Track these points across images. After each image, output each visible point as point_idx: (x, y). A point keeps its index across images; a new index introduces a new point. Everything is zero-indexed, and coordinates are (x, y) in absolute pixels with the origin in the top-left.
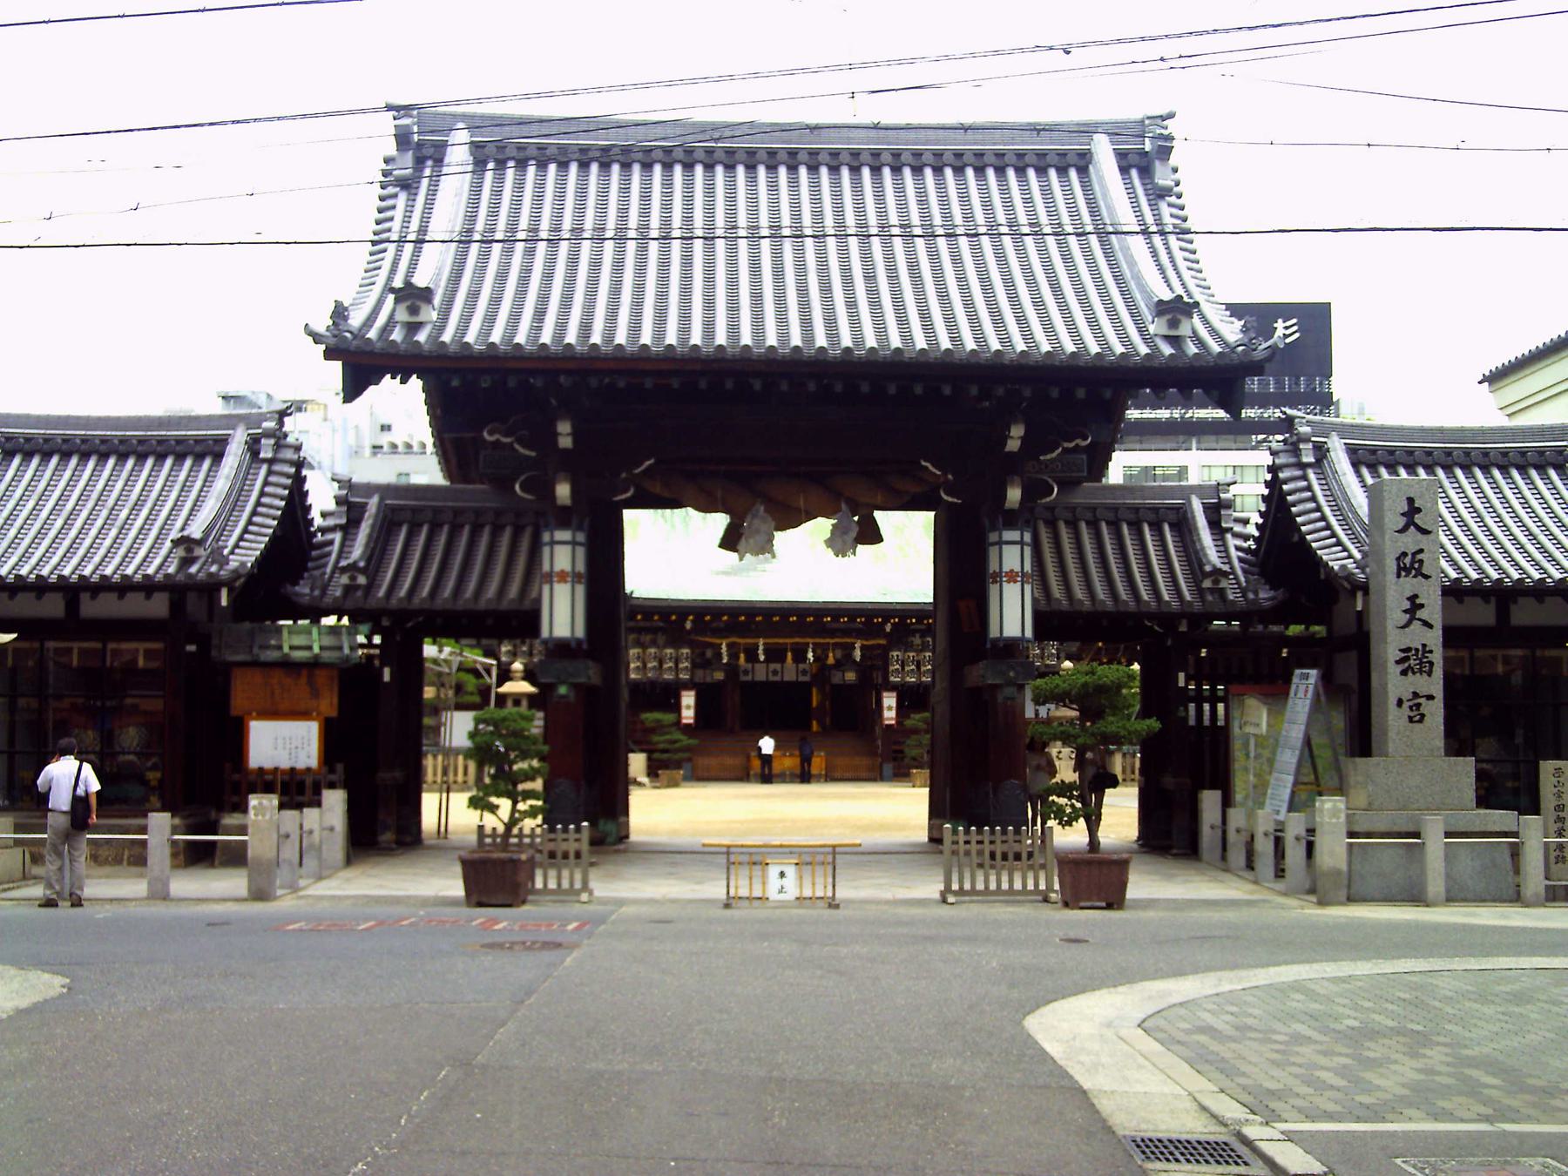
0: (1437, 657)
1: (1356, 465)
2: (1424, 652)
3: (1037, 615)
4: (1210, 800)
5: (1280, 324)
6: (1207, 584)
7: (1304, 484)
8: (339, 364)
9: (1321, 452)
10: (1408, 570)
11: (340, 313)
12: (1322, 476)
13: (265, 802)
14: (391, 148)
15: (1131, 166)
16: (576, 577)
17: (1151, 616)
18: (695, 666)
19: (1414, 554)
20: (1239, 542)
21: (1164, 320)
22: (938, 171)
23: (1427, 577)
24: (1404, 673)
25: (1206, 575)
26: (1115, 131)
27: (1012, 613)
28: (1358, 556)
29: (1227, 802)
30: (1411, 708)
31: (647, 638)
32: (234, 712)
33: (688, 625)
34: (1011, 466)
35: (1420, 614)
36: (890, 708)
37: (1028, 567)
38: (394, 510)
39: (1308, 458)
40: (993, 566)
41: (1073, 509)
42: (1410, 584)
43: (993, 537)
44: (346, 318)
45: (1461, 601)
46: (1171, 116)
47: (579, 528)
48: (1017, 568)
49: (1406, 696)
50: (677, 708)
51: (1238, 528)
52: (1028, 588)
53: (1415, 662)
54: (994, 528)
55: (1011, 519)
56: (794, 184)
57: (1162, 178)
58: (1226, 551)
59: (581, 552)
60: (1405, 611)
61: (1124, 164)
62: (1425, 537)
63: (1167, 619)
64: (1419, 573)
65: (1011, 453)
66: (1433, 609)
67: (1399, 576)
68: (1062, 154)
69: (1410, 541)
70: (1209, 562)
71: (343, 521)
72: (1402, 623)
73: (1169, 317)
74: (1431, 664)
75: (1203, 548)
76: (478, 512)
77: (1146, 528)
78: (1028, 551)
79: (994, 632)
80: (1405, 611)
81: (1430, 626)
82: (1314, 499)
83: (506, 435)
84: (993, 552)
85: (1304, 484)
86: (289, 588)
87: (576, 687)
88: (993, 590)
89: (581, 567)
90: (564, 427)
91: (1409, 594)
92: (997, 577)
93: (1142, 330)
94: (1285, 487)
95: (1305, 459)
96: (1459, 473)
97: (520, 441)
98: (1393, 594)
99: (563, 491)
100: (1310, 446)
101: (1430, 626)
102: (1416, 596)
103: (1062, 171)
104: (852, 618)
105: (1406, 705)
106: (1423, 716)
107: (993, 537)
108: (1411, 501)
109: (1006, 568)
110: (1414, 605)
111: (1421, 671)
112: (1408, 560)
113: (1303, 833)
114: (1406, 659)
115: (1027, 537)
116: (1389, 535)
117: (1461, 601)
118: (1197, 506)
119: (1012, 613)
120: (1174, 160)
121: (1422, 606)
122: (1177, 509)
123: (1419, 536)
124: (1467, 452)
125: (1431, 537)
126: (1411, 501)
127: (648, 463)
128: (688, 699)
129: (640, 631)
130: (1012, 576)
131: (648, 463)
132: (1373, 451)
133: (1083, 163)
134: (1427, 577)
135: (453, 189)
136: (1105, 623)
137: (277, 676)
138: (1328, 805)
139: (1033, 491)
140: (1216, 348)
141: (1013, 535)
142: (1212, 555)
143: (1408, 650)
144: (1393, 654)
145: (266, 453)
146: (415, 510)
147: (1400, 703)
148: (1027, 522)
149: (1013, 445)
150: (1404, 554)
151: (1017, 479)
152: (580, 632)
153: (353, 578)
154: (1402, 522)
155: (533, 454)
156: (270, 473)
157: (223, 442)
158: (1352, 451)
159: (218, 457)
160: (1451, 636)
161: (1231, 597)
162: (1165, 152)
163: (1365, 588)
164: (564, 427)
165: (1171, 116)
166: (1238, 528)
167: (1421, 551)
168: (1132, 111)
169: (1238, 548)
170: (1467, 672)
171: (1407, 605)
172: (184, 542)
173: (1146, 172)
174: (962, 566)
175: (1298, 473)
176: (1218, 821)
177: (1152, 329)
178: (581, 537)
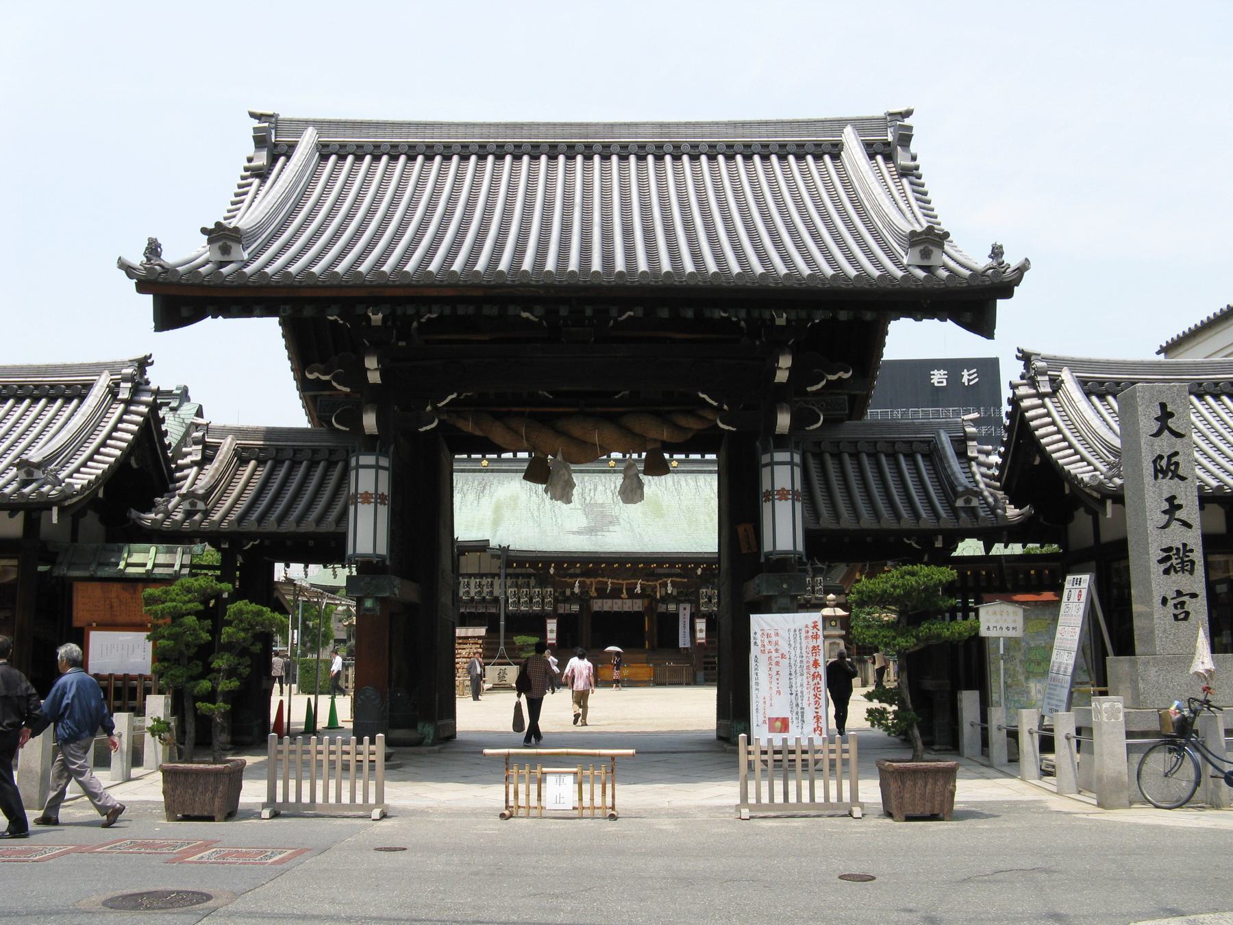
0: (1198, 556)
1: (1088, 394)
2: (1185, 551)
3: (809, 535)
4: (969, 701)
5: (965, 373)
6: (960, 503)
8: (150, 297)
9: (1056, 384)
11: (153, 249)
14: (250, 148)
16: (379, 499)
17: (909, 533)
18: (556, 600)
19: (1170, 457)
20: (984, 470)
22: (712, 158)
23: (1183, 479)
24: (1166, 572)
25: (957, 495)
26: (860, 124)
27: (783, 530)
28: (1104, 469)
29: (985, 704)
30: (1175, 606)
31: (520, 581)
33: (552, 571)
34: (781, 395)
35: (1179, 514)
36: (701, 631)
37: (798, 486)
38: (245, 448)
39: (1045, 388)
40: (766, 486)
42: (1168, 486)
43: (765, 459)
44: (158, 255)
46: (908, 113)
47: (385, 454)
48: (789, 487)
49: (1171, 594)
50: (543, 632)
52: (798, 505)
53: (1175, 560)
54: (766, 451)
55: (782, 442)
56: (587, 170)
57: (903, 160)
59: (384, 476)
60: (1165, 512)
62: (1179, 440)
66: (1190, 510)
67: (1156, 477)
68: (818, 145)
69: (1165, 444)
70: (961, 485)
71: (199, 458)
74: (1193, 563)
75: (954, 473)
76: (315, 451)
77: (902, 458)
78: (797, 471)
79: (767, 547)
80: (1165, 512)
81: (1190, 526)
83: (324, 374)
84: (765, 472)
85: (1042, 411)
86: (134, 513)
87: (382, 601)
88: (766, 508)
89: (384, 488)
90: (371, 363)
91: (1166, 495)
92: (770, 496)
93: (897, 263)
97: (335, 378)
98: (1152, 496)
99: (370, 421)
100: (1047, 378)
101: (1190, 526)
103: (818, 157)
104: (672, 565)
105: (1171, 603)
106: (1187, 614)
107: (765, 459)
108: (1163, 406)
109: (777, 487)
110: (1173, 506)
111: (1183, 570)
113: (1073, 733)
114: (1168, 558)
115: (797, 458)
116: (1144, 439)
118: (945, 438)
119: (783, 530)
120: (914, 147)
122: (928, 442)
123: (1174, 439)
125: (1185, 440)
126: (1163, 406)
127: (450, 397)
128: (552, 625)
129: (517, 576)
130: (783, 494)
131: (450, 397)
132: (1101, 383)
133: (836, 151)
134: (1183, 479)
135: (288, 173)
137: (116, 588)
138: (1106, 705)
139: (798, 421)
141: (781, 456)
142: (962, 478)
143: (1169, 549)
144: (1155, 554)
145: (124, 395)
147: (1164, 601)
148: (797, 447)
149: (782, 376)
150: (1161, 457)
152: (383, 549)
153: (193, 504)
154: (1155, 426)
155: (348, 390)
156: (126, 412)
157: (88, 386)
158: (1083, 383)
159: (82, 398)
160: (1210, 542)
161: (982, 514)
162: (905, 138)
163: (1118, 498)
164: (371, 363)
165: (908, 113)
167: (1176, 454)
168: (878, 110)
169: (983, 475)
171: (1166, 506)
172: (23, 464)
174: (740, 507)
175: (1036, 401)
176: (978, 720)
177: (905, 261)
178: (384, 462)
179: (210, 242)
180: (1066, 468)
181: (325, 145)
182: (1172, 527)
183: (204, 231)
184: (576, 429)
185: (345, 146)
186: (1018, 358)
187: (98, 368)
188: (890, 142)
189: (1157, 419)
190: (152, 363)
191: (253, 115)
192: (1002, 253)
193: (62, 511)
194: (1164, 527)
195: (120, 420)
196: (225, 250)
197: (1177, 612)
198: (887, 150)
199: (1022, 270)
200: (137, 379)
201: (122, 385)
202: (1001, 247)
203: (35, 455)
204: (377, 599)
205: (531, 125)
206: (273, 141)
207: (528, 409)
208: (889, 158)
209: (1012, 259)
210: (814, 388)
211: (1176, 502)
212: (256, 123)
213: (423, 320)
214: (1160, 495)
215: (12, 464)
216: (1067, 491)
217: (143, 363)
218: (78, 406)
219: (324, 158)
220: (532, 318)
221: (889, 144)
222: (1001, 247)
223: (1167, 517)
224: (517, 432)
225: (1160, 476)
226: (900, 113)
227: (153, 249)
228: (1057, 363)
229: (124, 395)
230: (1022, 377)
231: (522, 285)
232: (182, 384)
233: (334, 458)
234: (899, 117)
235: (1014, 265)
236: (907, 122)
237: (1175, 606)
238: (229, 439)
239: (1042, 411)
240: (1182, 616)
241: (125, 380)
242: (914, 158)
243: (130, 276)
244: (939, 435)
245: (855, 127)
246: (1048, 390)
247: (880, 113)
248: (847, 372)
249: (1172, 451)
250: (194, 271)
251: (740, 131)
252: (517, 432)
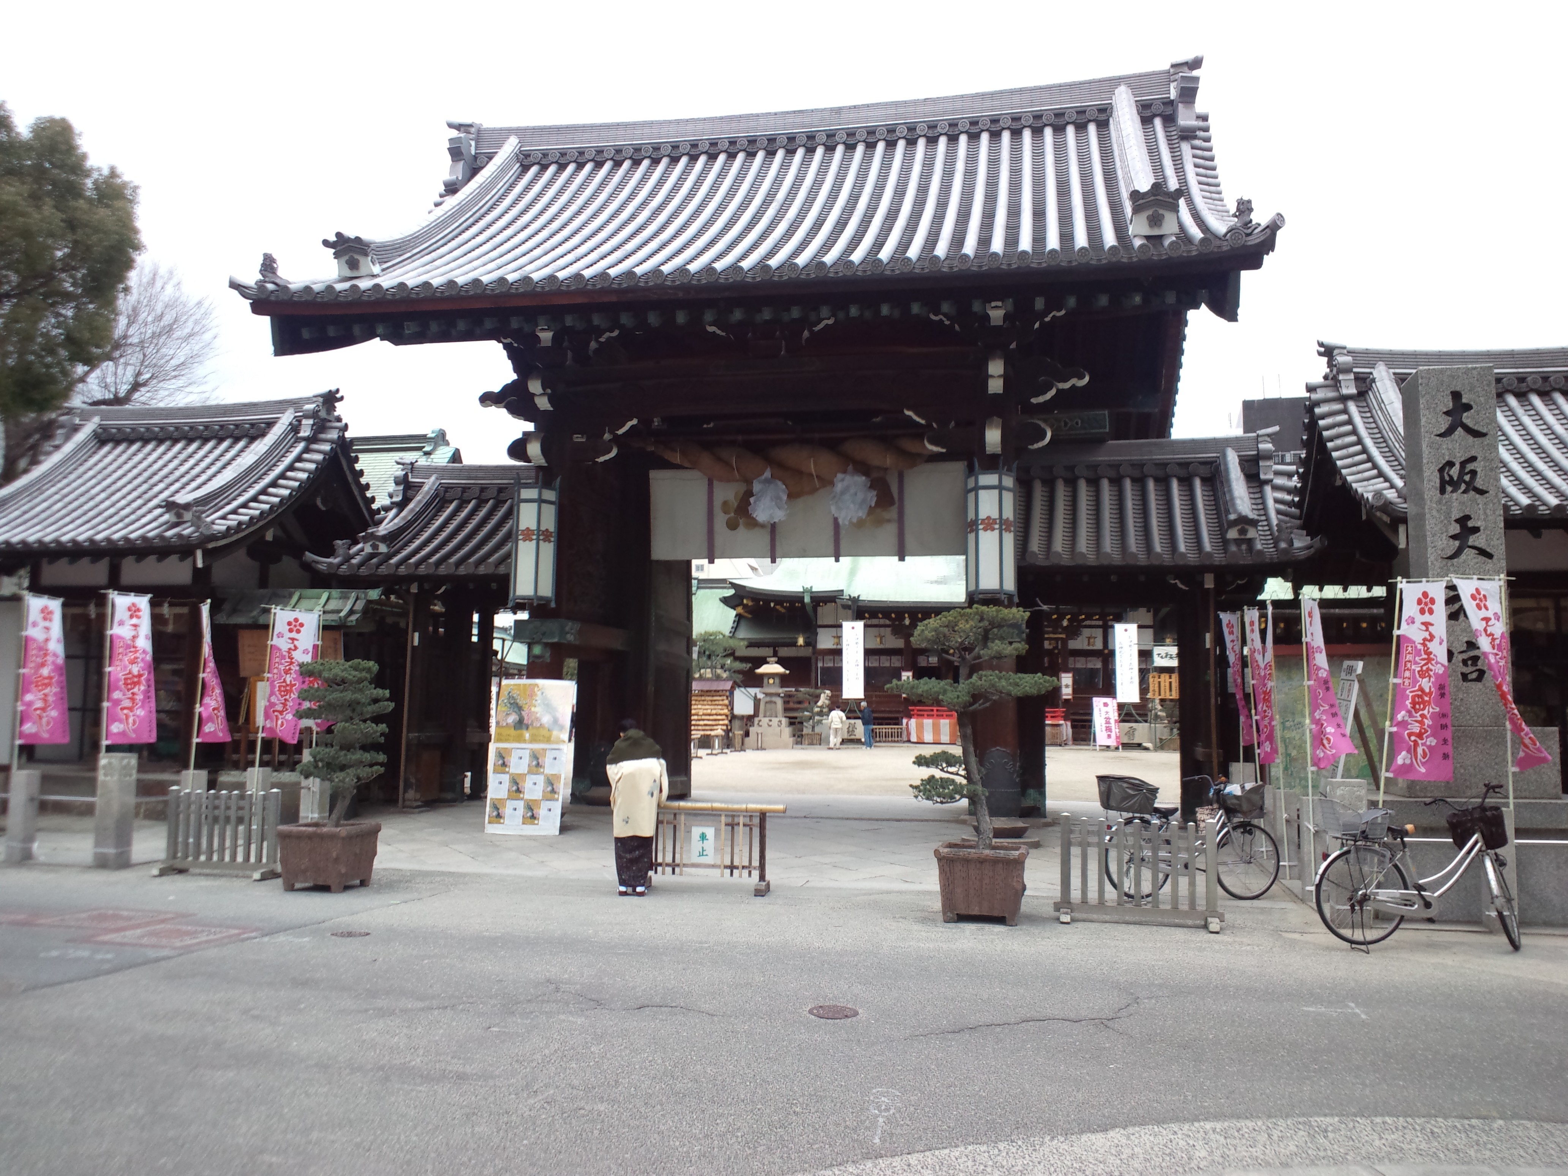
6: (1233, 534)
7: (1344, 417)
9: (1365, 384)
10: (1455, 484)
11: (268, 265)
12: (1367, 410)
13: (113, 760)
15: (1155, 116)
16: (542, 535)
19: (1463, 464)
21: (1143, 218)
23: (1482, 492)
26: (1135, 82)
28: (1400, 483)
30: (1465, 662)
32: (243, 674)
36: (1067, 686)
39: (1349, 388)
41: (1094, 467)
42: (1459, 502)
45: (1538, 535)
48: (995, 515)
51: (1279, 481)
57: (1185, 119)
58: (1264, 503)
60: (1454, 537)
61: (1148, 113)
62: (1477, 441)
63: (1190, 574)
64: (1471, 487)
65: (996, 395)
67: (1443, 491)
69: (1458, 446)
70: (1235, 511)
72: (1450, 553)
73: (1150, 212)
80: (1454, 537)
81: (1490, 556)
82: (1354, 432)
85: (1344, 417)
94: (1321, 423)
95: (1345, 391)
96: (1535, 400)
100: (1352, 376)
101: (1490, 556)
102: (1467, 518)
106: (1481, 673)
108: (1456, 396)
109: (982, 515)
110: (1466, 529)
112: (1455, 472)
117: (1538, 535)
118: (1232, 459)
120: (1200, 105)
121: (1476, 530)
123: (1470, 439)
124: (1545, 378)
126: (1456, 396)
127: (629, 424)
130: (989, 524)
131: (629, 424)
133: (1102, 118)
134: (1482, 492)
136: (1113, 578)
140: (1196, 233)
141: (991, 479)
145: (305, 432)
146: (465, 489)
149: (995, 386)
150: (1450, 464)
151: (998, 421)
153: (375, 547)
154: (1444, 423)
156: (307, 450)
157: (270, 424)
162: (1189, 93)
165: (1196, 63)
166: (1279, 481)
167: (1473, 459)
170: (1552, 627)
171: (1456, 529)
173: (1169, 120)
175: (1338, 406)
178: (550, 495)
179: (337, 255)
180: (1354, 485)
181: (527, 156)
182: (1463, 557)
183: (326, 243)
184: (792, 456)
185: (549, 155)
186: (1320, 354)
187: (282, 405)
188: (1170, 105)
189: (1447, 413)
190: (342, 398)
191: (451, 126)
192: (1251, 210)
193: (206, 554)
194: (1451, 558)
195: (299, 459)
196: (353, 265)
197: (1466, 670)
198: (1169, 111)
199: (1274, 227)
200: (323, 414)
201: (304, 422)
202: (1249, 202)
203: (183, 498)
204: (546, 645)
205: (748, 117)
206: (469, 152)
207: (740, 438)
208: (1169, 120)
209: (1260, 217)
210: (1041, 399)
211: (1470, 524)
212: (454, 133)
213: (602, 340)
214: (1448, 515)
215: (159, 506)
216: (1364, 517)
217: (331, 399)
218: (246, 447)
219: (525, 168)
220: (719, 332)
221: (1171, 103)
222: (1249, 202)
223: (1457, 543)
224: (728, 464)
225: (1449, 489)
226: (1186, 64)
227: (268, 265)
228: (1371, 357)
229: (305, 432)
230: (1326, 377)
231: (657, 287)
232: (437, 428)
233: (485, 496)
234: (1186, 69)
235: (1264, 222)
236: (1195, 73)
237: (1465, 662)
238: (433, 478)
239: (1343, 417)
240: (1474, 675)
241: (306, 417)
242: (1205, 118)
243: (245, 296)
244: (1224, 455)
245: (1129, 85)
246: (1353, 391)
247: (1164, 65)
248: (1081, 377)
249: (1467, 456)
250: (330, 288)
251: (988, 103)
252: (728, 464)
